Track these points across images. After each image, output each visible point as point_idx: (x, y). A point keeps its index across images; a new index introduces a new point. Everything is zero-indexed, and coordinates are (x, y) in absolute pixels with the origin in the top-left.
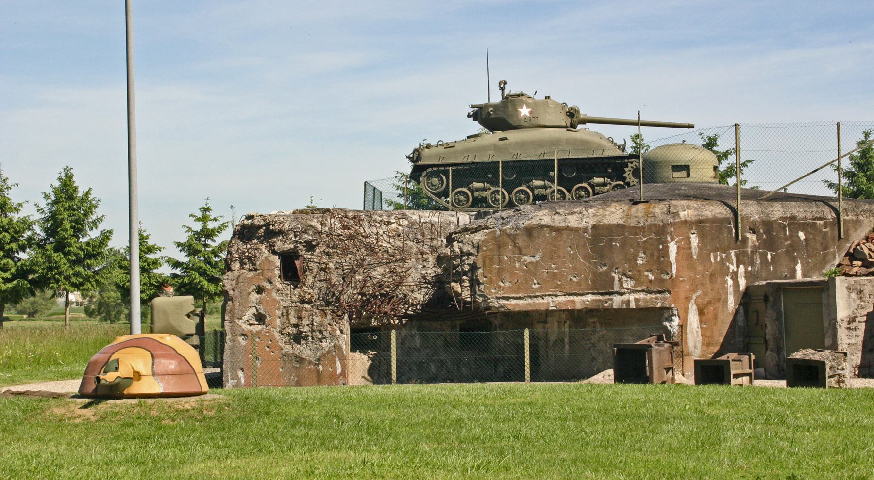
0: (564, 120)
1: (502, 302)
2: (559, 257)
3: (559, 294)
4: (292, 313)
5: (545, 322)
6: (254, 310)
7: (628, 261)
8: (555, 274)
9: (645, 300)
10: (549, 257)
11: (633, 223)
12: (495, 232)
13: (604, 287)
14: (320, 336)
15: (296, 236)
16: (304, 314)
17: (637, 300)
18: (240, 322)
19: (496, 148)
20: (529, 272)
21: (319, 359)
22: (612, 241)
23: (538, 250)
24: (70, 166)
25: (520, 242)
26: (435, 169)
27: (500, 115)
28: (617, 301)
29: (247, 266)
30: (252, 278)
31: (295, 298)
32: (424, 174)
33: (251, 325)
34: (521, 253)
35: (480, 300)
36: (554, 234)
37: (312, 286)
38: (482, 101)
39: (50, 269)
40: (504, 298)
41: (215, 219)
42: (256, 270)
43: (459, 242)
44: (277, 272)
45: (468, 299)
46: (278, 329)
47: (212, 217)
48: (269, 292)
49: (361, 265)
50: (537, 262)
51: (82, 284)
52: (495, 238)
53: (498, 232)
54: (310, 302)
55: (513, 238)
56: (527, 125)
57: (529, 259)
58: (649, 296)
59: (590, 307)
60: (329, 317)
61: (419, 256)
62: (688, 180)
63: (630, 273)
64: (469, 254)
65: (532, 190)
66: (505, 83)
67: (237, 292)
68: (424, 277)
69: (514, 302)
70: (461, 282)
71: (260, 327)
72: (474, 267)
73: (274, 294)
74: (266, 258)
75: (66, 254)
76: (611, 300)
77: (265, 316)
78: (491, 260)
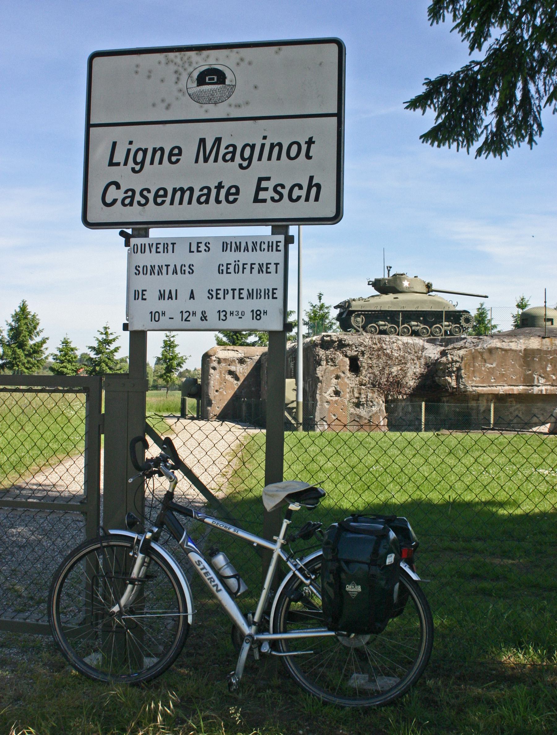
0: (425, 290)
1: (474, 388)
2: (506, 365)
3: (505, 385)
4: (356, 390)
5: (478, 400)
6: (334, 389)
7: (543, 369)
8: (503, 374)
9: (551, 390)
10: (500, 365)
11: (545, 348)
12: (471, 350)
13: (529, 381)
14: (371, 404)
15: (356, 348)
16: (362, 391)
17: (546, 390)
18: (325, 395)
19: (392, 303)
20: (489, 372)
21: (370, 417)
22: (534, 357)
23: (495, 361)
24: (25, 299)
25: (486, 356)
26: (359, 313)
27: (392, 284)
28: (536, 390)
29: (330, 364)
30: (333, 370)
31: (357, 383)
32: (354, 315)
33: (331, 396)
34: (485, 362)
35: (462, 387)
36: (503, 352)
37: (365, 375)
38: (380, 276)
39: (15, 358)
40: (475, 386)
41: (111, 334)
42: (336, 366)
43: (451, 355)
44: (348, 368)
45: (455, 386)
46: (348, 399)
47: (109, 333)
48: (343, 379)
49: (386, 366)
50: (494, 367)
51: (31, 368)
52: (471, 353)
53: (473, 350)
54: (365, 385)
55: (481, 354)
56: (406, 291)
57: (489, 366)
58: (552, 388)
59: (521, 392)
60: (376, 393)
61: (412, 361)
62: (552, 326)
63: (543, 375)
64: (457, 362)
65: (411, 327)
66: (391, 267)
67: (324, 378)
68: (415, 373)
69: (480, 388)
70: (451, 377)
71: (337, 398)
72: (459, 369)
73: (346, 380)
74: (342, 359)
75: (24, 350)
76: (533, 389)
77: (340, 392)
78: (469, 366)
